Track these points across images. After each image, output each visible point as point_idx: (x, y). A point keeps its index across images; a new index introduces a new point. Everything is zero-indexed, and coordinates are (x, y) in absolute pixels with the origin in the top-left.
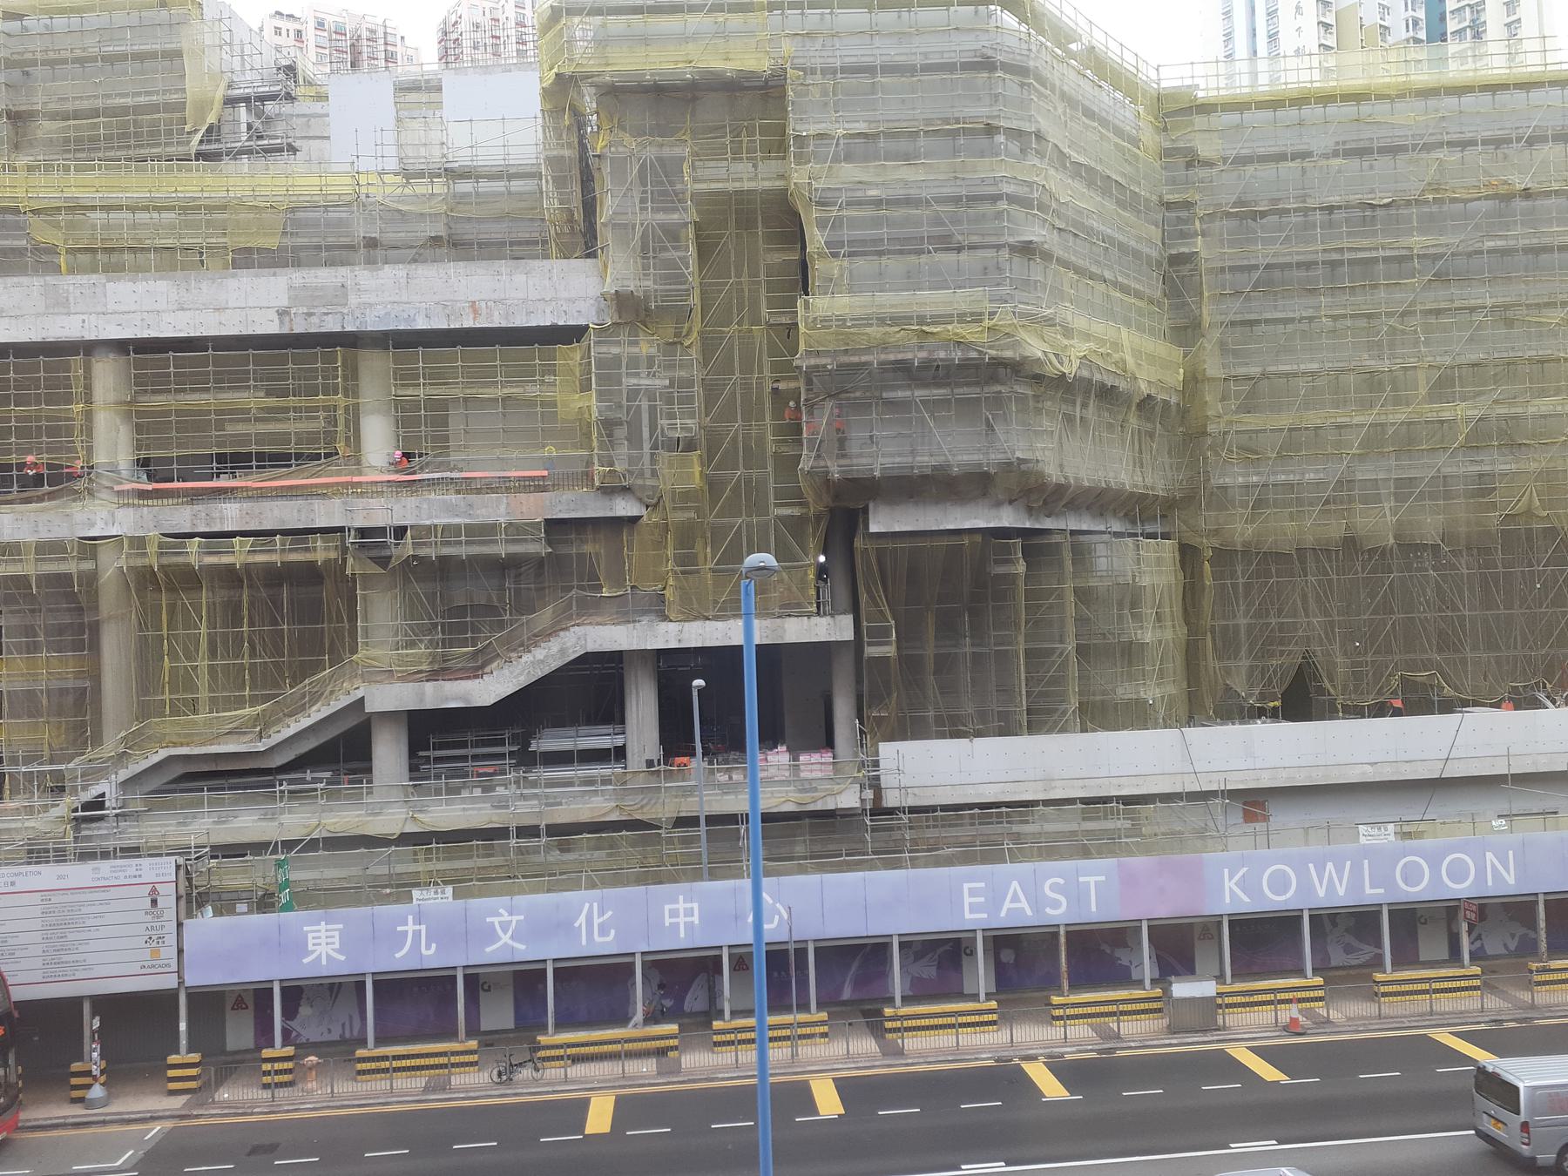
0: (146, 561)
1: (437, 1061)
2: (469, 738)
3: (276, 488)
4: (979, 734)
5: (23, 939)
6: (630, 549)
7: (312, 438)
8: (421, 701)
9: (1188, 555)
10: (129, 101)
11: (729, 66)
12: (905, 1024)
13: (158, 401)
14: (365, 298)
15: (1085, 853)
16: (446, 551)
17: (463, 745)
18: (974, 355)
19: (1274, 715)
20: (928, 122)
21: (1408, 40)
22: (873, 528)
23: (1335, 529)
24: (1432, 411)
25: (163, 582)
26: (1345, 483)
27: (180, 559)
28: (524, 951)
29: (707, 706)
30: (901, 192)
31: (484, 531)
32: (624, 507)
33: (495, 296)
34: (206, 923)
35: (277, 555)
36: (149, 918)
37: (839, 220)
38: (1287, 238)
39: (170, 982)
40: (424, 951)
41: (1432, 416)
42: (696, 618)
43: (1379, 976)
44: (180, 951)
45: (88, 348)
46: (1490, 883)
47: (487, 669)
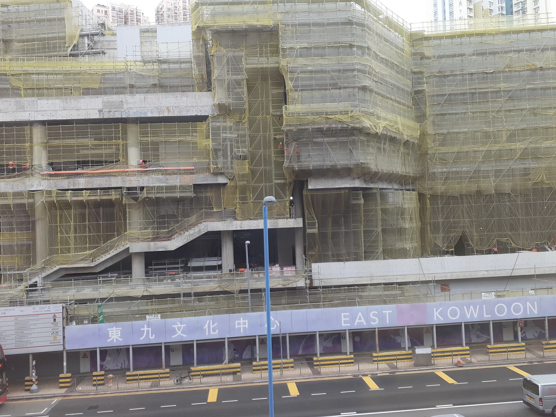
0: (52, 199)
1: (155, 376)
2: (166, 262)
3: (98, 173)
4: (347, 260)
5: (8, 333)
6: (224, 195)
7: (111, 155)
8: (149, 248)
9: (421, 197)
10: (46, 36)
11: (258, 23)
12: (321, 363)
13: (56, 142)
14: (130, 106)
15: (385, 302)
16: (158, 195)
17: (164, 264)
18: (345, 126)
19: (452, 254)
20: (329, 43)
21: (499, 14)
22: (310, 187)
23: (473, 188)
24: (508, 146)
25: (58, 207)
26: (477, 171)
27: (64, 198)
28: (186, 337)
29: (251, 250)
30: (319, 68)
31: (172, 188)
32: (221, 180)
33: (176, 105)
34: (73, 327)
35: (98, 197)
36: (53, 325)
37: (297, 78)
38: (457, 85)
39: (60, 348)
40: (150, 337)
41: (508, 148)
42: (247, 219)
43: (489, 346)
44: (64, 337)
45: (31, 123)
46: (528, 313)
47: (173, 237)
